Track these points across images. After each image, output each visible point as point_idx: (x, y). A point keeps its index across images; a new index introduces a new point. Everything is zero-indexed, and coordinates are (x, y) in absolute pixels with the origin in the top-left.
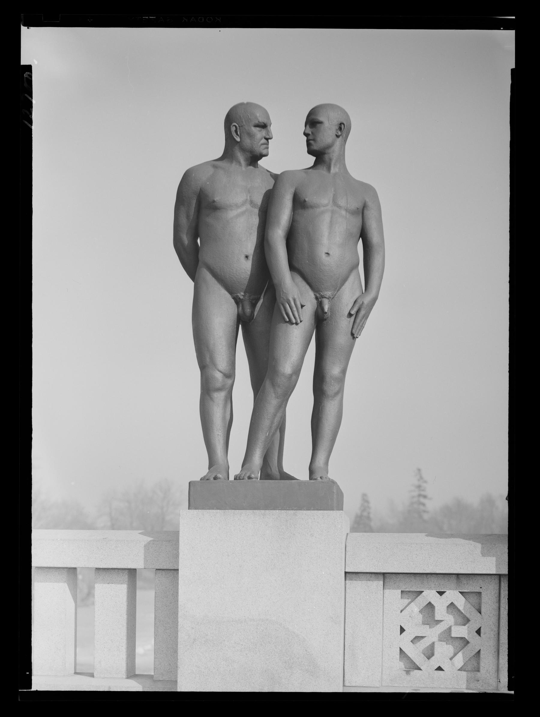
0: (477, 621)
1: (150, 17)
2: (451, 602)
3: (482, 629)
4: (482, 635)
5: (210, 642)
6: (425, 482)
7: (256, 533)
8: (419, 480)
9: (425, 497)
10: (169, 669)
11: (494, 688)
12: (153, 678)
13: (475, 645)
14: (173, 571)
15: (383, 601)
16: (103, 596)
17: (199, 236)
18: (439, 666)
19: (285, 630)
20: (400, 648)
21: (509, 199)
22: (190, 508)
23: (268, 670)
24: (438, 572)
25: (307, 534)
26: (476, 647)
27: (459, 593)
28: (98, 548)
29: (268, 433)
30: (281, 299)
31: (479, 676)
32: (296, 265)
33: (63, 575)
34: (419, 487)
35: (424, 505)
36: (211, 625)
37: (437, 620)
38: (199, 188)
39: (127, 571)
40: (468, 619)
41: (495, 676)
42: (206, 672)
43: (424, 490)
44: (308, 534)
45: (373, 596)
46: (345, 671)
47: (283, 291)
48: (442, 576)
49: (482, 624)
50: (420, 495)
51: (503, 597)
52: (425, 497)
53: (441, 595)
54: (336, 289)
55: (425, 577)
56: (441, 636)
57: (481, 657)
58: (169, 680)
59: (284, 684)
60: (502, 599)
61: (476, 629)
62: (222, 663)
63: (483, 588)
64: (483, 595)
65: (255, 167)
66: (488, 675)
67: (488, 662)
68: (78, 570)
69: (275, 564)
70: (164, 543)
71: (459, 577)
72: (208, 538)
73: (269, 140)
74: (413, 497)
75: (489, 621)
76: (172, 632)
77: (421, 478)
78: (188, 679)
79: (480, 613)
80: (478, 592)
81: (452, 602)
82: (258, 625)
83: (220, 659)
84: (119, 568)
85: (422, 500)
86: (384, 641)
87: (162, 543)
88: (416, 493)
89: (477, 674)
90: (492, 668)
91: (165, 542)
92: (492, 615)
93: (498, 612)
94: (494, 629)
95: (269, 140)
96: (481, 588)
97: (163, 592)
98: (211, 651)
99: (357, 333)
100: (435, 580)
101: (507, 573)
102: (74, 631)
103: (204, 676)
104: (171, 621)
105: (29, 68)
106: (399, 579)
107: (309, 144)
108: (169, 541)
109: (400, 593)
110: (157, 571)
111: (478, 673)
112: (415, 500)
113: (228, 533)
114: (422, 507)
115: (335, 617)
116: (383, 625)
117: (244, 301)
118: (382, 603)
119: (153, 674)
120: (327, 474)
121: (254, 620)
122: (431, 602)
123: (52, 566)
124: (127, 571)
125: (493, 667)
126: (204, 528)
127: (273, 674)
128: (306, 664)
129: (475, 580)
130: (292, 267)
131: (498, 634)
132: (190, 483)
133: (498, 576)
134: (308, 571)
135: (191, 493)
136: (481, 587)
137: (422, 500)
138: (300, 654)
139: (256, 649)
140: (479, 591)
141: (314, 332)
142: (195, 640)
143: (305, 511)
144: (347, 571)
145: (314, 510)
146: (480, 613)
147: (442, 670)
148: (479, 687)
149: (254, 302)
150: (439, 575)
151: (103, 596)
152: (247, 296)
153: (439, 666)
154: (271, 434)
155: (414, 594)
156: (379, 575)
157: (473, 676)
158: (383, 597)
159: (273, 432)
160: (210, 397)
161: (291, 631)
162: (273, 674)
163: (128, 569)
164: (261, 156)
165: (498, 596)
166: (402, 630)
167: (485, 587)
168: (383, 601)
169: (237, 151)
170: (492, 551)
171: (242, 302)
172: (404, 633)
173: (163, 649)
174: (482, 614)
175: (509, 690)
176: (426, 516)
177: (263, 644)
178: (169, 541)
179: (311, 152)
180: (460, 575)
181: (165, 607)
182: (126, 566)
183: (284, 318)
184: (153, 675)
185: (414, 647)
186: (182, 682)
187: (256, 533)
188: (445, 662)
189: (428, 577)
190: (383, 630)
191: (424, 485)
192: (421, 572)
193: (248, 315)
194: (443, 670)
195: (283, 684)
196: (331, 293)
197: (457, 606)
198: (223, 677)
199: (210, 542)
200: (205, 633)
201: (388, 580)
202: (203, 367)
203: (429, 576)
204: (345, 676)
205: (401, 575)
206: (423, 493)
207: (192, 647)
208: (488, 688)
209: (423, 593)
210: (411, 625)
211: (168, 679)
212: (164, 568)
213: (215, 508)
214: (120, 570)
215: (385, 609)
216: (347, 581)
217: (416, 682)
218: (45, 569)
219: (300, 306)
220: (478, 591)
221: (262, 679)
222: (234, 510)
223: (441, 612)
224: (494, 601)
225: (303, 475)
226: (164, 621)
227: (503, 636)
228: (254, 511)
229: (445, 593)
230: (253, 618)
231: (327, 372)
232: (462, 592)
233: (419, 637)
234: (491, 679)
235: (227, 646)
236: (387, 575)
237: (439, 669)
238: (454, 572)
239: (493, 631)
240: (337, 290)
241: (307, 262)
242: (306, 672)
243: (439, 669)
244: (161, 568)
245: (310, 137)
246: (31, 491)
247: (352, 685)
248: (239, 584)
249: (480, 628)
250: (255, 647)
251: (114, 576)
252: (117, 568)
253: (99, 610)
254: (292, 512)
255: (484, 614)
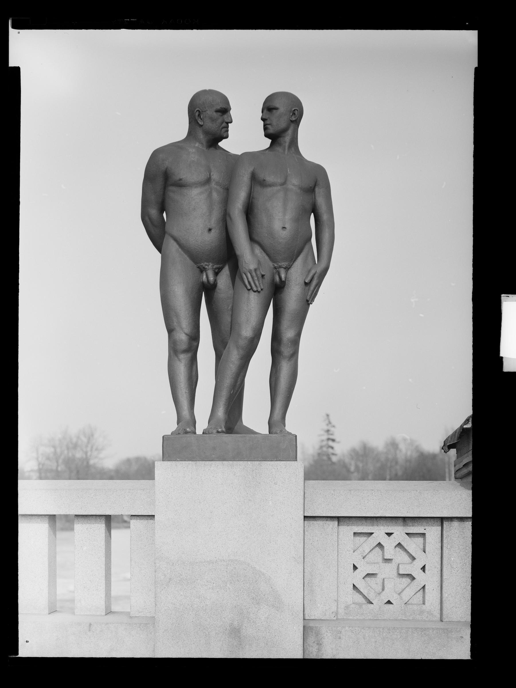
0: (422, 560)
1: (132, 20)
2: (398, 542)
3: (426, 566)
4: (426, 571)
5: (184, 581)
6: (334, 426)
7: (225, 482)
8: (327, 425)
9: (333, 440)
10: (144, 606)
11: (438, 619)
12: (130, 614)
13: (421, 581)
14: (147, 517)
15: (338, 542)
16: (82, 540)
17: (165, 210)
18: (389, 600)
19: (252, 569)
20: (353, 584)
21: (472, 408)
22: (164, 459)
23: (238, 606)
24: (387, 516)
25: (271, 483)
26: (422, 583)
27: (405, 534)
28: (78, 496)
29: (232, 391)
30: (244, 269)
31: (424, 609)
32: (256, 238)
33: (45, 521)
34: (328, 431)
35: (332, 448)
36: (185, 566)
37: (386, 559)
38: (166, 167)
39: (104, 517)
40: (414, 557)
41: (438, 609)
42: (181, 609)
43: (332, 434)
44: (272, 482)
45: (329, 538)
46: (305, 606)
47: (245, 262)
48: (390, 519)
49: (427, 562)
50: (328, 439)
51: (446, 538)
52: (333, 440)
53: (389, 536)
54: (292, 260)
55: (375, 520)
56: (390, 573)
57: (426, 591)
58: (144, 616)
59: (252, 618)
60: (444, 539)
61: (422, 567)
62: (196, 600)
63: (427, 529)
64: (427, 536)
65: (216, 149)
66: (432, 607)
67: (432, 596)
68: (57, 516)
69: (243, 510)
70: (139, 491)
71: (405, 520)
72: (182, 487)
73: (229, 124)
74: (322, 441)
75: (433, 559)
76: (147, 573)
77: (330, 423)
78: (164, 615)
79: (425, 552)
80: (422, 533)
81: (399, 543)
82: (228, 565)
83: (194, 596)
84: (98, 514)
85: (331, 443)
86: (339, 578)
87: (137, 491)
88: (325, 437)
89: (423, 607)
90: (436, 601)
91: (139, 490)
92: (435, 553)
93: (440, 551)
94: (437, 566)
95: (229, 124)
96: (425, 529)
97: (138, 536)
98: (185, 589)
99: (311, 300)
100: (384, 523)
101: (470, 515)
102: (444, 586)
103: (179, 612)
104: (146, 562)
105: (502, 358)
106: (351, 522)
107: (265, 129)
108: (144, 490)
109: (353, 535)
110: (132, 517)
111: (424, 606)
112: (325, 443)
113: (199, 483)
114: (330, 450)
115: (297, 557)
116: (338, 563)
117: (208, 270)
118: (337, 544)
119: (130, 611)
120: (285, 427)
121: (224, 560)
122: (380, 542)
123: (35, 513)
124: (104, 518)
125: (436, 600)
126: (178, 478)
127: (242, 610)
128: (272, 600)
129: (420, 522)
130: (252, 239)
131: (440, 571)
132: (163, 437)
133: (440, 519)
134: (272, 516)
135: (164, 446)
136: (425, 528)
137: (331, 443)
138: (267, 591)
139: (226, 587)
140: (423, 533)
141: (272, 299)
142: (170, 579)
143: (269, 462)
144: (306, 515)
145: (277, 461)
146: (425, 552)
147: (391, 603)
148: (425, 618)
149: (217, 271)
150: (388, 518)
151: (82, 540)
152: (210, 265)
153: (389, 600)
154: (235, 392)
155: (365, 535)
156: (334, 519)
157: (419, 608)
158: (338, 539)
159: (236, 390)
160: (178, 358)
161: (258, 570)
162: (242, 610)
163: (105, 515)
164: (221, 138)
165: (441, 536)
166: (355, 568)
167: (429, 528)
168: (338, 542)
169: (200, 134)
170: (435, 497)
171: (206, 271)
172: (357, 571)
173: (139, 588)
174: (426, 553)
175: (471, 658)
176: (334, 459)
177: (232, 582)
178: (144, 490)
179: (267, 135)
180: (406, 518)
181: (140, 549)
182: (105, 513)
183: (246, 287)
184: (130, 612)
185: (366, 584)
186: (159, 618)
187: (225, 482)
188: (394, 596)
189: (377, 520)
190: (338, 569)
191: (332, 429)
192: (372, 516)
193: (211, 283)
194: (392, 604)
195: (251, 618)
196: (288, 264)
197: (404, 546)
198: (196, 613)
199: (183, 490)
200: (180, 573)
201: (342, 523)
202: (170, 331)
203: (378, 519)
204: (305, 610)
205: (353, 518)
206: (331, 437)
207: (168, 586)
208: (432, 619)
209: (373, 535)
210: (363, 564)
211: (143, 616)
212: (139, 514)
213: (187, 460)
214: (97, 517)
215: (339, 549)
216: (113, 532)
217: (368, 614)
218: (28, 516)
219: (260, 276)
220: (422, 532)
221: (232, 614)
222: (205, 462)
223: (390, 551)
224: (437, 541)
225: (263, 429)
226: (139, 562)
227: (446, 573)
228: (223, 462)
229: (393, 534)
230: (224, 559)
231: (284, 335)
232: (408, 533)
233: (370, 574)
234: (435, 610)
235: (200, 585)
236: (340, 519)
237: (389, 602)
238: (402, 516)
239: (436, 568)
240: (293, 261)
241: (266, 235)
242: (272, 607)
243: (389, 602)
244: (137, 514)
245: (268, 122)
246: (473, 504)
247: (311, 618)
248: (210, 528)
249: (425, 565)
250: (225, 585)
251: (92, 522)
252: (96, 514)
253: (79, 554)
254: (257, 463)
255: (428, 553)
